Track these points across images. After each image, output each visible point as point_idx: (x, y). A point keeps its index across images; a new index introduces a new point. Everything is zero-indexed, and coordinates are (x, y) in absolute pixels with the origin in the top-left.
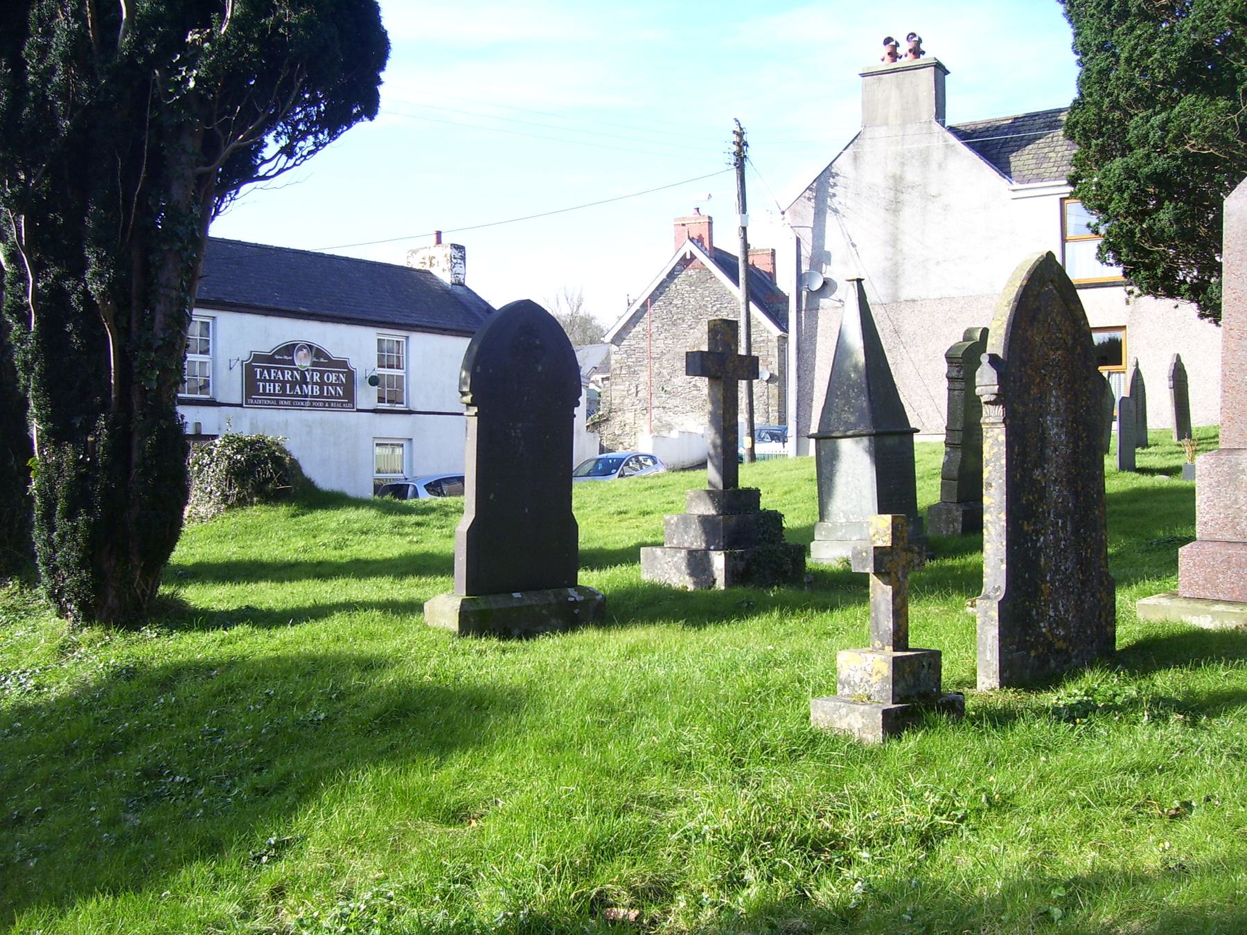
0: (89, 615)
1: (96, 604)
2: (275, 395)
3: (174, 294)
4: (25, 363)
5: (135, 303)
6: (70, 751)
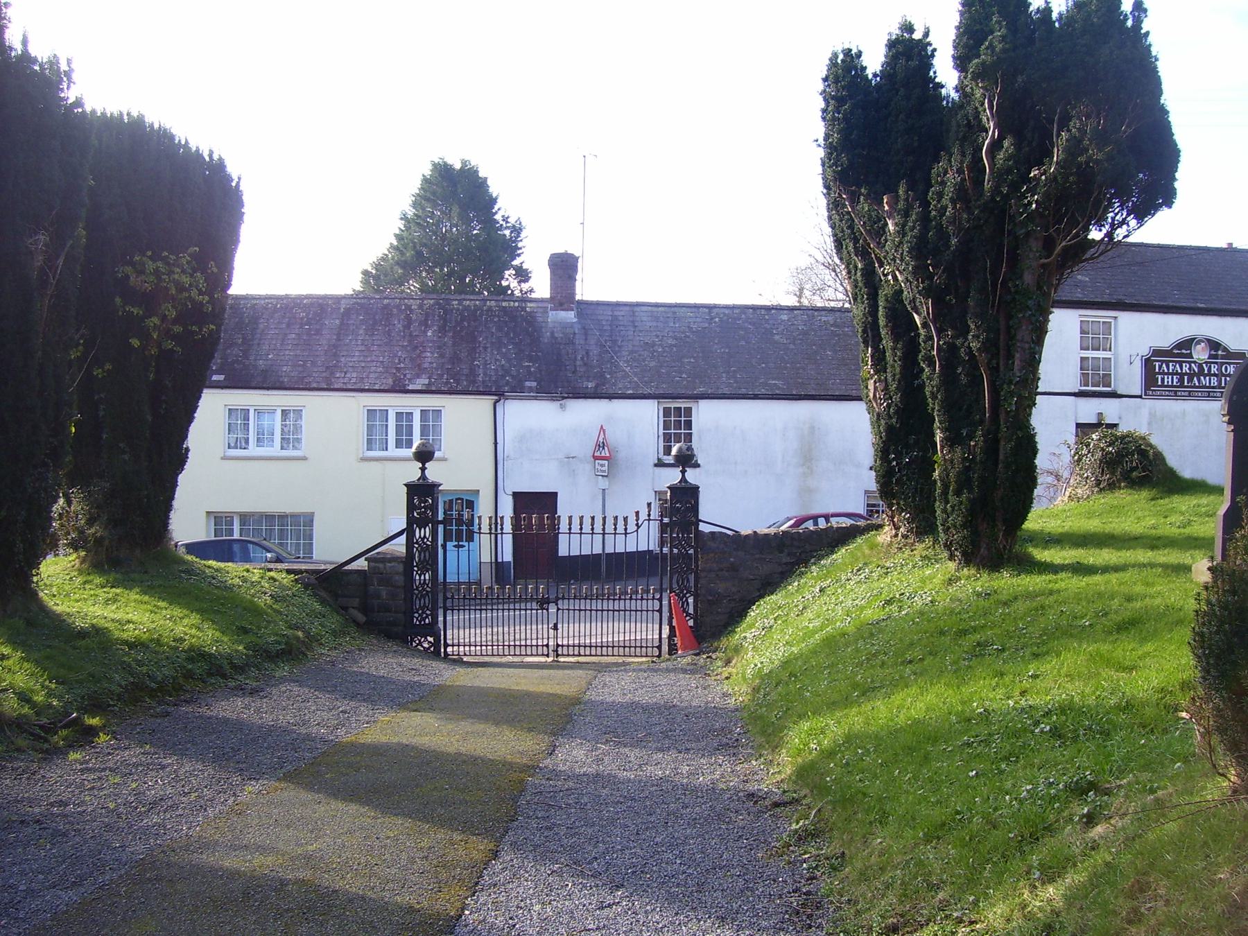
0: (969, 558)
1: (972, 553)
2: (1172, 386)
3: (1027, 346)
4: (932, 393)
5: (1002, 352)
6: (942, 633)
